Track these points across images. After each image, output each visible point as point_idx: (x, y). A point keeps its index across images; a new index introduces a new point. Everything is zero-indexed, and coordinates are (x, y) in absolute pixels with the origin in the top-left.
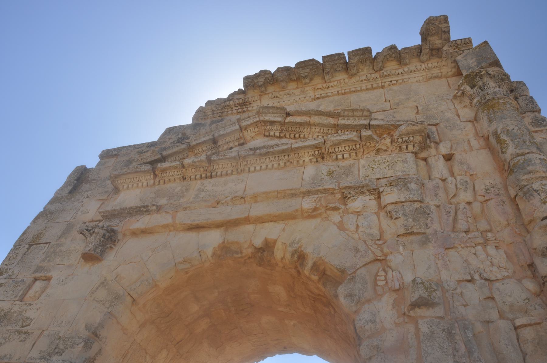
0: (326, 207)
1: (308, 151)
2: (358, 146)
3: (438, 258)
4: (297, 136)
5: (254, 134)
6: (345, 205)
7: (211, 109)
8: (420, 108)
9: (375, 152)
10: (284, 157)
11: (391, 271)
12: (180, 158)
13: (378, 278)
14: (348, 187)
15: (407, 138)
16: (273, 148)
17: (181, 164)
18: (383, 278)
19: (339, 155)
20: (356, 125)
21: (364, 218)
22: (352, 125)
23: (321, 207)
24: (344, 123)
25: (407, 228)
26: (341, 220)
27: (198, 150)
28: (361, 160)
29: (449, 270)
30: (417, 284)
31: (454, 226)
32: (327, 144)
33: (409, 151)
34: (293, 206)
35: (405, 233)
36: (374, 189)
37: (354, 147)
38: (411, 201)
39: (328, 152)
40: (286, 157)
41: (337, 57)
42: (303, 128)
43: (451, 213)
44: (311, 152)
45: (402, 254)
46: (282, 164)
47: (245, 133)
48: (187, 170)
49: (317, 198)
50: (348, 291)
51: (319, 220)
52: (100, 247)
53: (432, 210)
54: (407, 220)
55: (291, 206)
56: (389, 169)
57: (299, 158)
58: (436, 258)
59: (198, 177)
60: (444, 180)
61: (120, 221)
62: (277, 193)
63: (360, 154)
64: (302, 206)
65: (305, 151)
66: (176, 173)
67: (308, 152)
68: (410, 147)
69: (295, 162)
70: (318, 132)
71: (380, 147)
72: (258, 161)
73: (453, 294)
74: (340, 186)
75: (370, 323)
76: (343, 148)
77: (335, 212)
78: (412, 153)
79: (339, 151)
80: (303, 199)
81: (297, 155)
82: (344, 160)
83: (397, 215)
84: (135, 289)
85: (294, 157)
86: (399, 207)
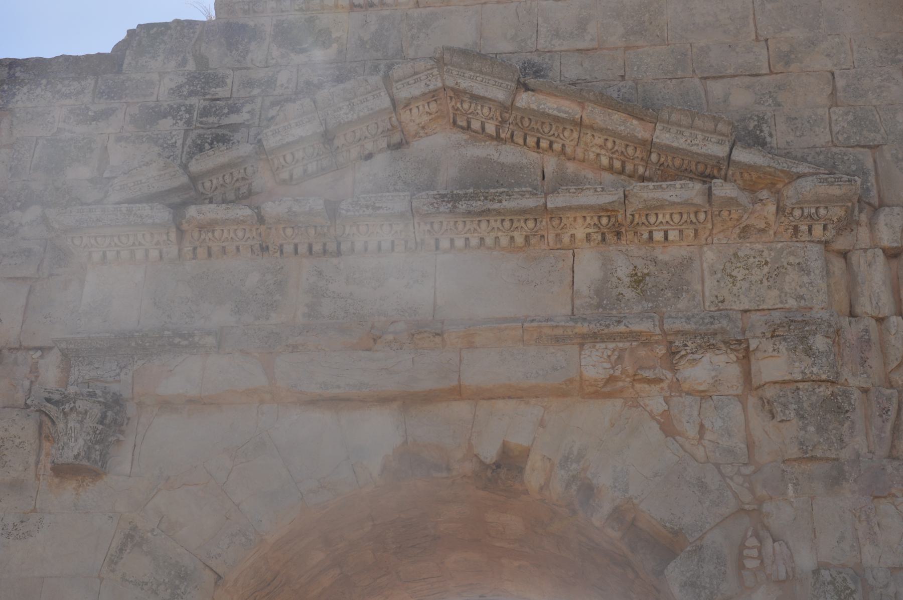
0: (635, 375)
1: (585, 214)
2: (702, 216)
3: (860, 516)
4: (544, 144)
5: (426, 118)
6: (673, 369)
8: (840, 83)
9: (737, 231)
10: (525, 223)
11: (770, 541)
12: (235, 179)
13: (746, 552)
14: (682, 331)
15: (813, 211)
16: (500, 201)
17: (255, 214)
18: (755, 553)
19: (655, 230)
20: (698, 153)
21: (715, 408)
22: (686, 150)
23: (624, 376)
24: (668, 143)
25: (805, 448)
26: (666, 408)
27: (282, 160)
28: (705, 249)
29: (877, 545)
30: (824, 584)
31: (892, 442)
32: (631, 203)
33: (814, 239)
34: (561, 368)
35: (800, 458)
36: (737, 340)
37: (692, 216)
38: (813, 381)
39: (632, 222)
40: (531, 224)
42: (561, 128)
43: (889, 413)
44: (592, 217)
45: (791, 503)
46: (520, 240)
47: (405, 116)
48: (270, 228)
49: (614, 350)
50: (688, 575)
51: (619, 402)
52: (97, 447)
53: (853, 402)
54: (804, 428)
55: (557, 370)
56: (769, 287)
57: (562, 228)
58: (855, 516)
59: (303, 249)
60: (880, 320)
61: (121, 368)
62: (521, 331)
63: (703, 235)
64: (581, 373)
65: (578, 215)
66: (240, 234)
67: (584, 217)
68: (818, 230)
69: (551, 237)
70: (600, 146)
71: (752, 221)
73: (881, 595)
74: (665, 328)
76: (668, 217)
77: (653, 386)
78: (819, 242)
79: (658, 222)
81: (556, 222)
82: (666, 244)
83: (784, 415)
84: (219, 555)
85: (550, 226)
86: (789, 393)
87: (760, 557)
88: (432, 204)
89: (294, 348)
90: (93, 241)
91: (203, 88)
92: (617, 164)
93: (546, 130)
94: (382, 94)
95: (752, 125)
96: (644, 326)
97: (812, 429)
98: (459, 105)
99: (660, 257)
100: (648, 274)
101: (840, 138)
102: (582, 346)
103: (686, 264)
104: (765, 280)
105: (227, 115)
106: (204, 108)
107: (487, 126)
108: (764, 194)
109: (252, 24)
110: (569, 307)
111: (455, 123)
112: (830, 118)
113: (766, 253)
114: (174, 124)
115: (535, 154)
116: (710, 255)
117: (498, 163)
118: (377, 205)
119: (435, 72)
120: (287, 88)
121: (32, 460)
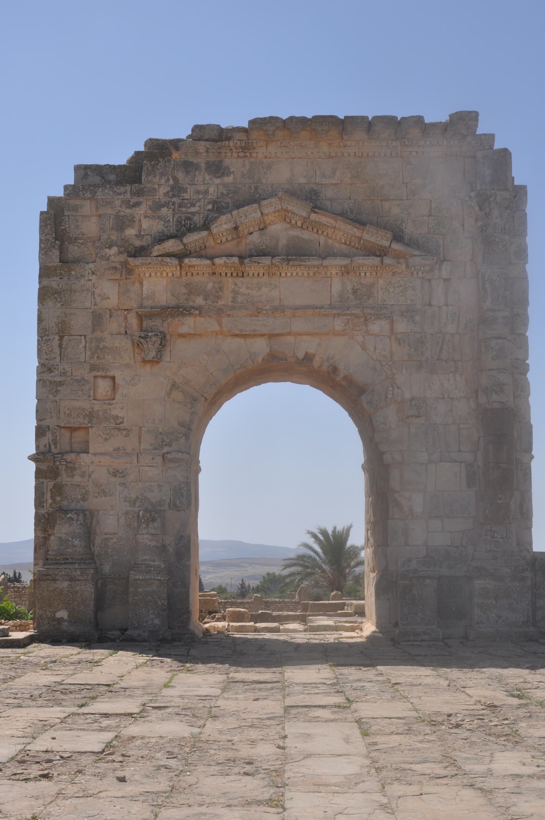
2: (379, 269)
4: (320, 232)
6: (366, 325)
7: (204, 147)
8: (434, 205)
11: (396, 388)
13: (388, 392)
15: (419, 268)
16: (305, 262)
18: (391, 392)
28: (379, 279)
41: (360, 120)
46: (311, 274)
56: (401, 296)
60: (439, 307)
61: (163, 322)
69: (323, 274)
72: (290, 269)
75: (383, 425)
76: (367, 268)
80: (334, 319)
87: (393, 394)
88: (280, 262)
89: (229, 315)
90: (146, 270)
91: (178, 193)
92: (348, 242)
93: (321, 227)
94: (258, 211)
95: (399, 223)
96: (357, 311)
97: (413, 350)
98: (287, 214)
99: (363, 282)
100: (358, 289)
101: (431, 231)
102: (334, 317)
103: (372, 285)
104: (400, 293)
105: (190, 207)
106: (180, 203)
107: (298, 223)
108: (402, 260)
109: (195, 162)
110: (330, 302)
111: (285, 220)
112: (428, 221)
113: (401, 282)
114: (168, 211)
115: (316, 235)
116: (381, 282)
117: (302, 238)
118: (259, 262)
119: (279, 202)
120: (213, 195)
121: (132, 355)
